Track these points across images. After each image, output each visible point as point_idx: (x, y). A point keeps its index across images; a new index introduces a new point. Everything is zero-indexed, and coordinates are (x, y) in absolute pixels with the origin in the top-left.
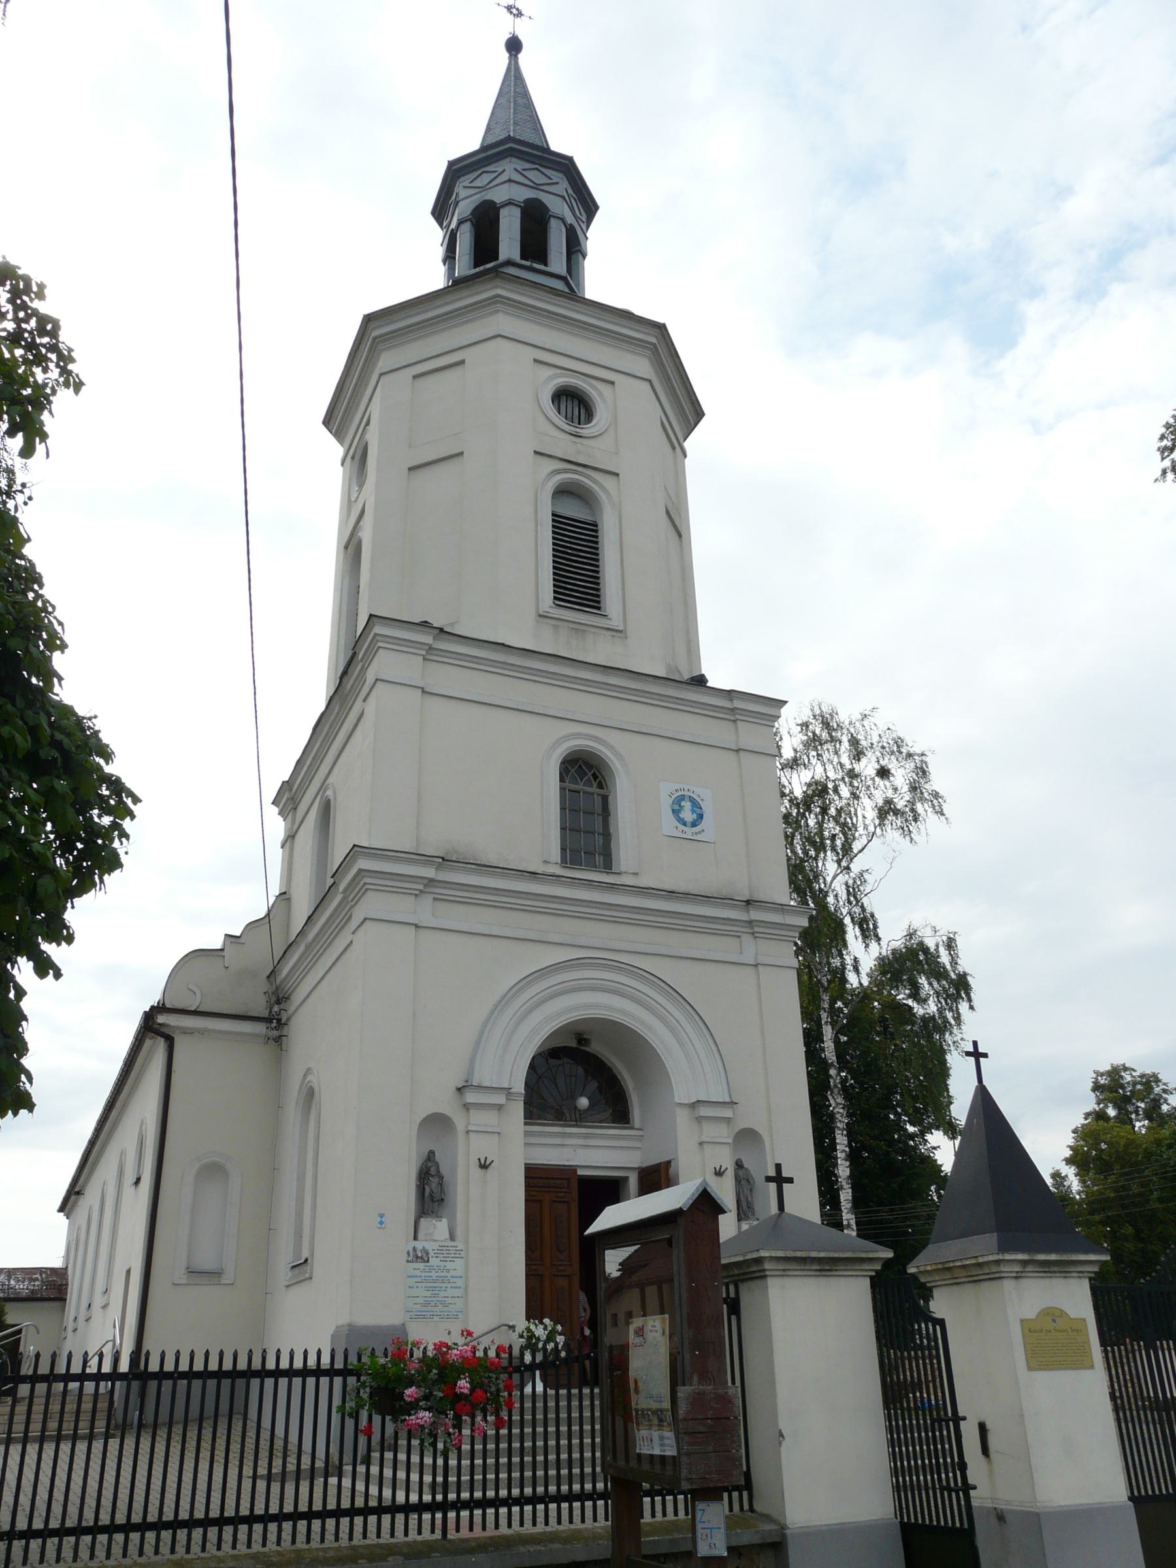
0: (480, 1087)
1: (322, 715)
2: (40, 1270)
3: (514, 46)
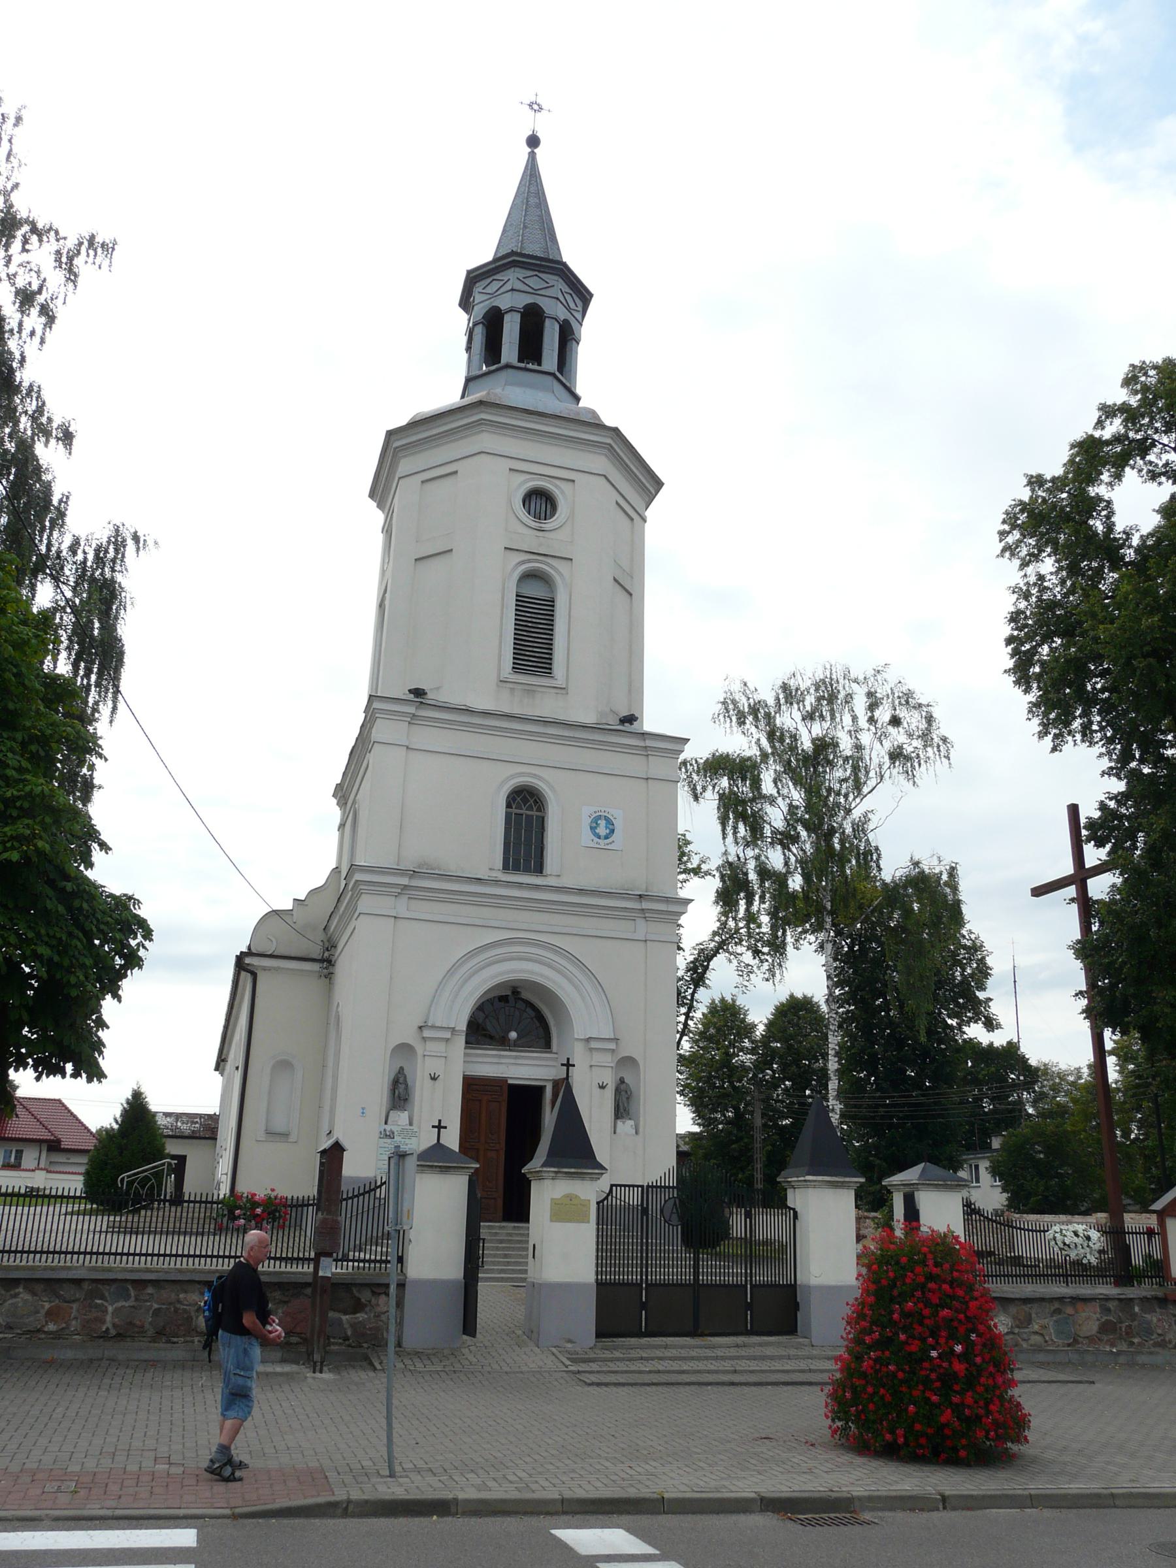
0: (433, 1027)
1: (354, 747)
2: (200, 1116)
3: (533, 141)
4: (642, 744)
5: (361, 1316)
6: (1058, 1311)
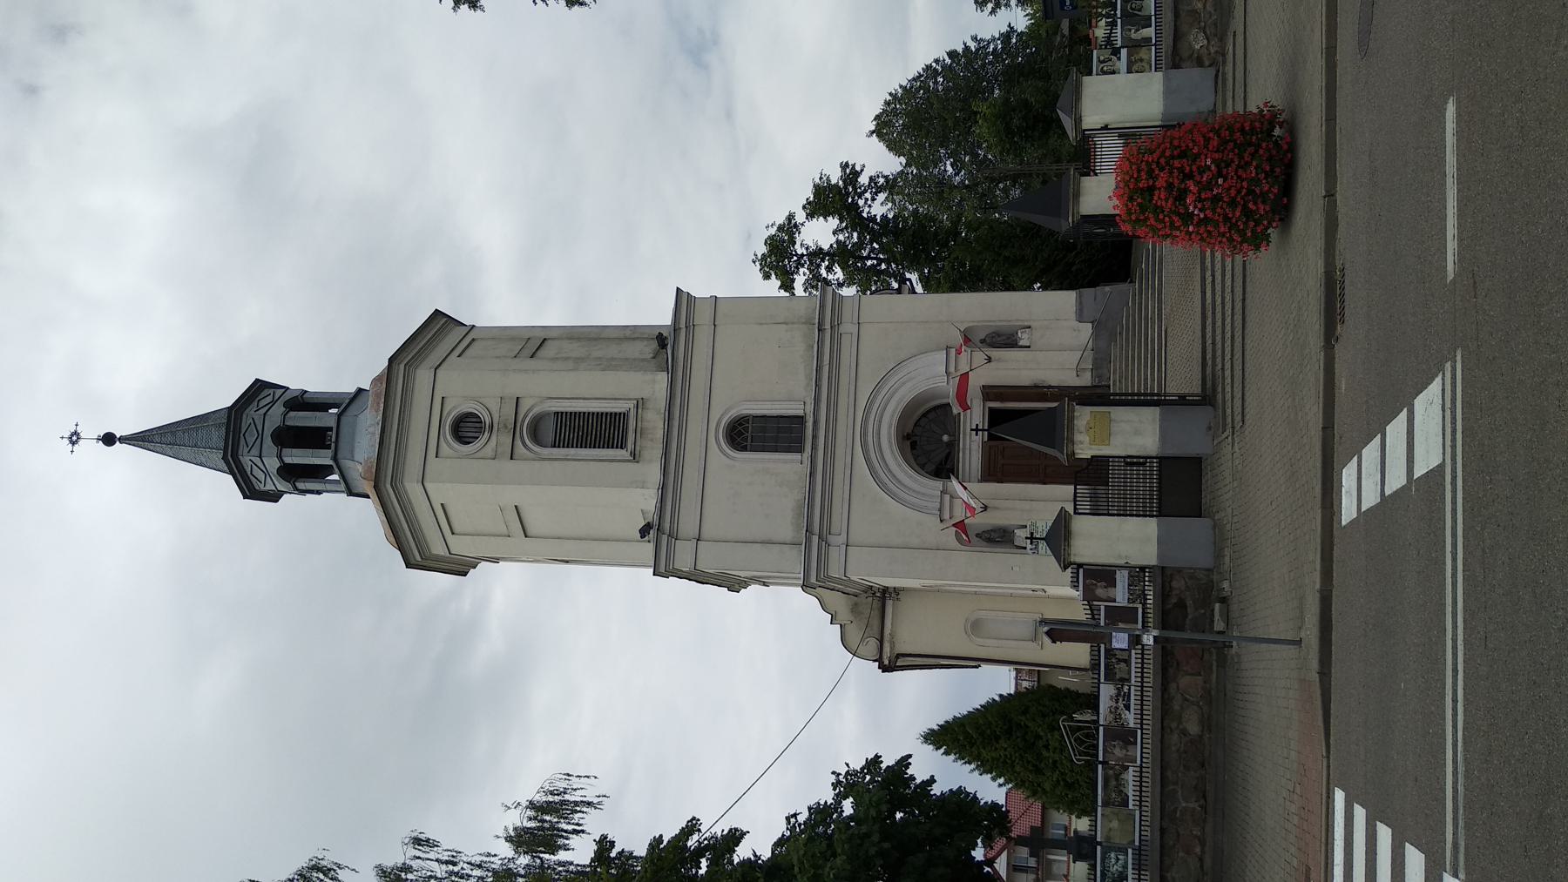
3: (109, 439)
5: (1189, 603)
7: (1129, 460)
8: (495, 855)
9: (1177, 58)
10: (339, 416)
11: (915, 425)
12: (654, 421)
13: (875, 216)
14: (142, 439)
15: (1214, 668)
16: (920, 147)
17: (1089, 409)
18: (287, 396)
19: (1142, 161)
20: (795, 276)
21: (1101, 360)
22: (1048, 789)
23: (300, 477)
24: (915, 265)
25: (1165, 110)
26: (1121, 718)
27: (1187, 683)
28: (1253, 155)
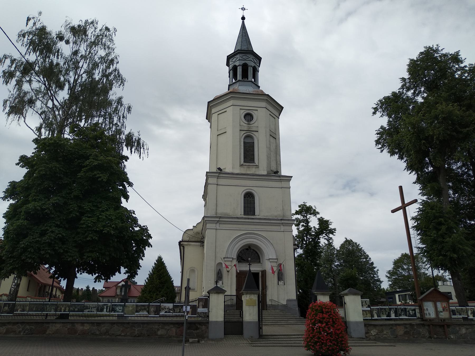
3: (243, 18)
4: (280, 179)
5: (198, 331)
6: (391, 328)
7: (241, 312)
8: (125, 129)
9: (368, 326)
10: (252, 81)
11: (253, 250)
12: (252, 171)
13: (320, 240)
14: (243, 27)
15: (178, 339)
16: (343, 254)
17: (257, 299)
18: (257, 67)
19: (331, 310)
20: (300, 215)
21: (275, 307)
22: (144, 295)
23: (234, 71)
24: (306, 252)
25: (351, 322)
26: (162, 310)
27: (173, 331)
28: (334, 344)
